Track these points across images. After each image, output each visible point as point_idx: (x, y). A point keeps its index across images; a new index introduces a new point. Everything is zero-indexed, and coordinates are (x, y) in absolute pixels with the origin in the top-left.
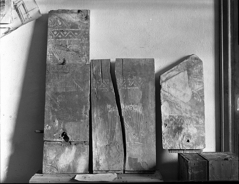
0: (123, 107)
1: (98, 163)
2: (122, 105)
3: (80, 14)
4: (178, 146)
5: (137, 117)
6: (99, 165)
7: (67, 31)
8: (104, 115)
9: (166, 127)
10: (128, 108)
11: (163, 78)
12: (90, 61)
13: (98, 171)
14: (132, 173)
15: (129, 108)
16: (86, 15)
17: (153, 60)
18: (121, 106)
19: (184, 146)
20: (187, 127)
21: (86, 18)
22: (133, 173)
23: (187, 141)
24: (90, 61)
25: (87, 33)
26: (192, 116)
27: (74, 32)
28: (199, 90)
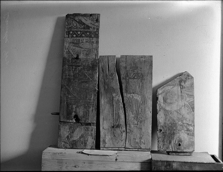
0: (125, 96)
1: (104, 141)
2: (125, 94)
3: (91, 17)
4: (171, 149)
5: (137, 104)
6: (106, 143)
7: (81, 31)
8: (111, 101)
9: (161, 132)
10: (129, 96)
11: (160, 91)
12: (99, 56)
13: (105, 148)
14: (128, 148)
15: (130, 96)
16: (96, 18)
17: (151, 57)
18: (124, 95)
19: (176, 148)
20: (179, 133)
21: (96, 20)
22: (128, 148)
23: (179, 145)
24: (99, 56)
25: (97, 33)
26: (184, 124)
27: (86, 32)
28: (190, 101)
